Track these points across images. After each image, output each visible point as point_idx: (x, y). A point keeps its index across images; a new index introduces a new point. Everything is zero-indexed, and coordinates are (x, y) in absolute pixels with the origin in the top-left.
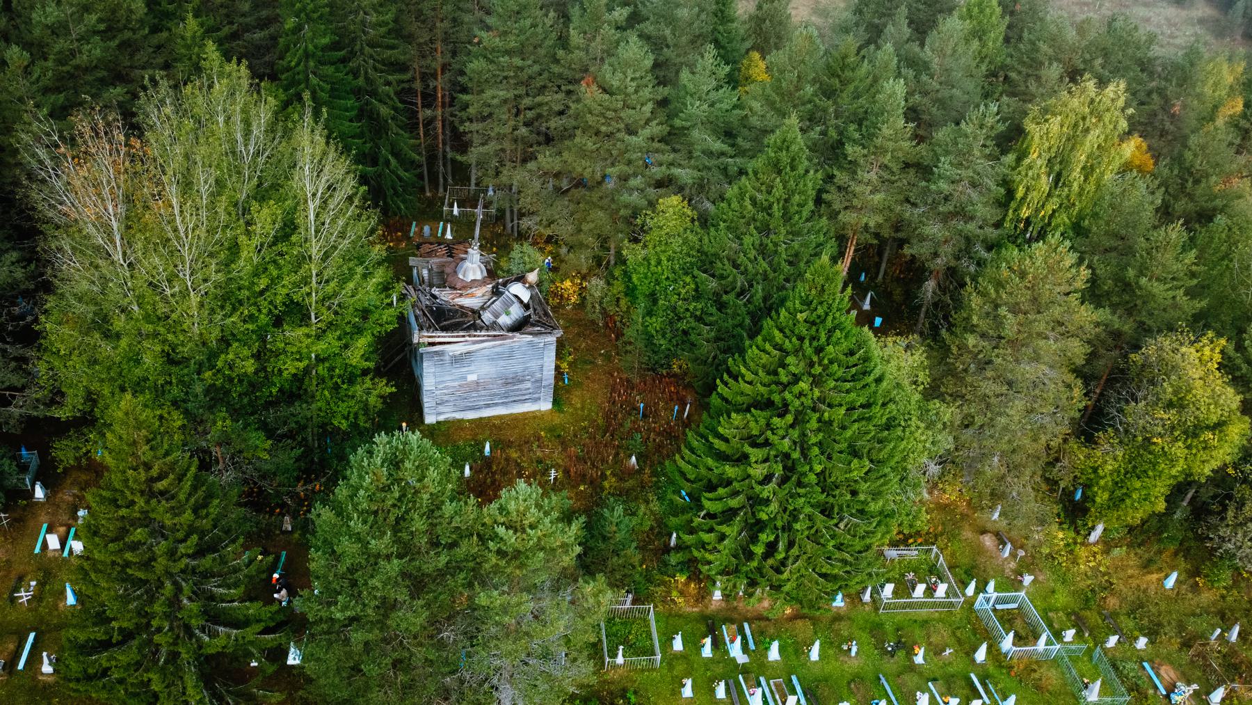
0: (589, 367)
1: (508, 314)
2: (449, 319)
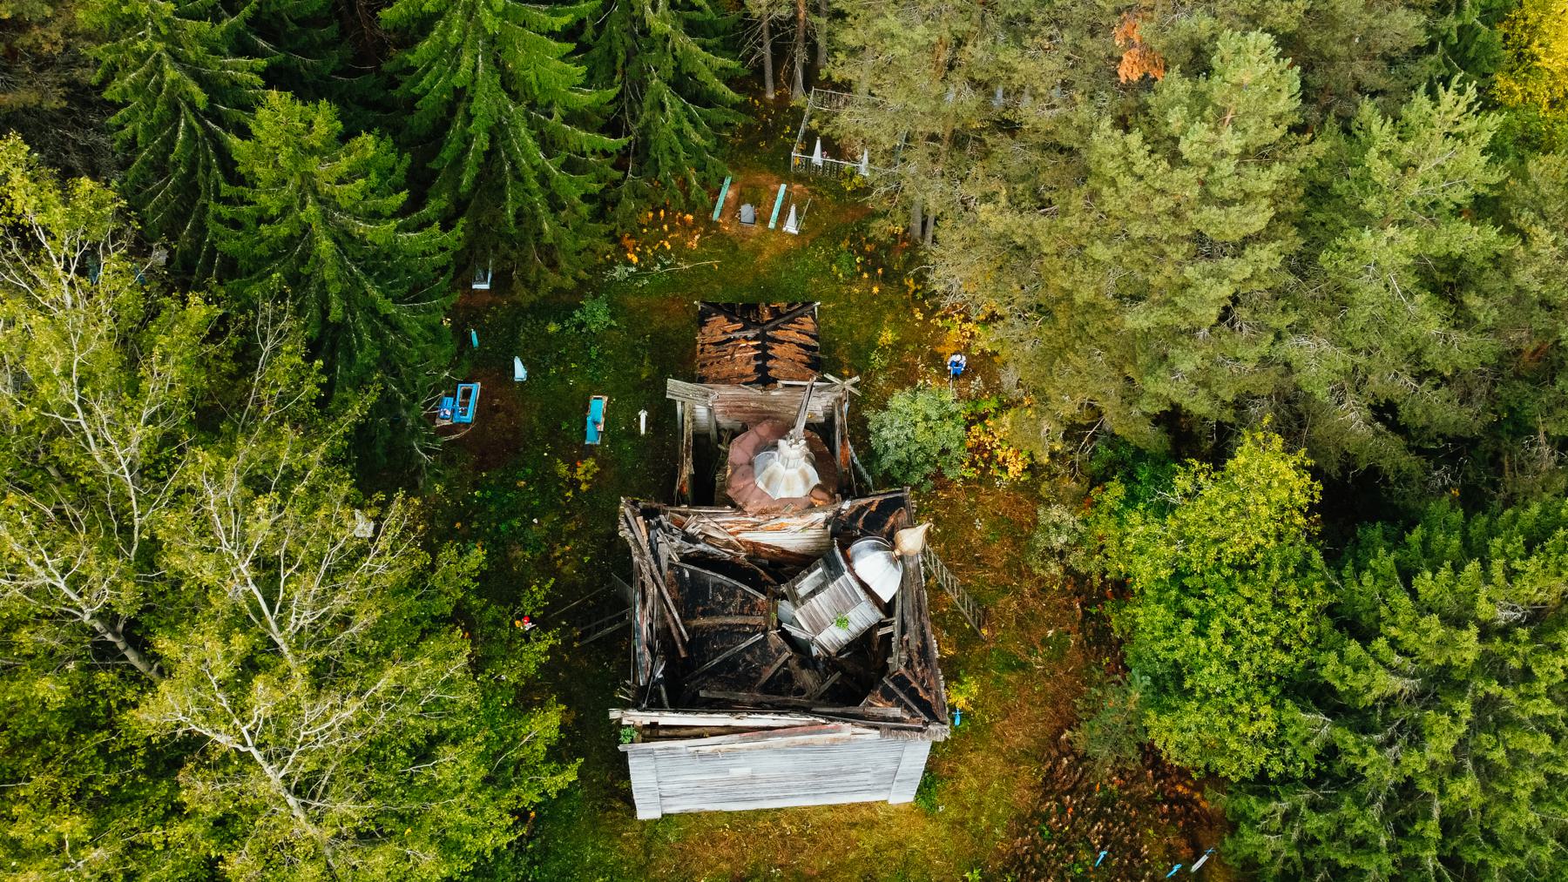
0: (1013, 678)
1: (842, 622)
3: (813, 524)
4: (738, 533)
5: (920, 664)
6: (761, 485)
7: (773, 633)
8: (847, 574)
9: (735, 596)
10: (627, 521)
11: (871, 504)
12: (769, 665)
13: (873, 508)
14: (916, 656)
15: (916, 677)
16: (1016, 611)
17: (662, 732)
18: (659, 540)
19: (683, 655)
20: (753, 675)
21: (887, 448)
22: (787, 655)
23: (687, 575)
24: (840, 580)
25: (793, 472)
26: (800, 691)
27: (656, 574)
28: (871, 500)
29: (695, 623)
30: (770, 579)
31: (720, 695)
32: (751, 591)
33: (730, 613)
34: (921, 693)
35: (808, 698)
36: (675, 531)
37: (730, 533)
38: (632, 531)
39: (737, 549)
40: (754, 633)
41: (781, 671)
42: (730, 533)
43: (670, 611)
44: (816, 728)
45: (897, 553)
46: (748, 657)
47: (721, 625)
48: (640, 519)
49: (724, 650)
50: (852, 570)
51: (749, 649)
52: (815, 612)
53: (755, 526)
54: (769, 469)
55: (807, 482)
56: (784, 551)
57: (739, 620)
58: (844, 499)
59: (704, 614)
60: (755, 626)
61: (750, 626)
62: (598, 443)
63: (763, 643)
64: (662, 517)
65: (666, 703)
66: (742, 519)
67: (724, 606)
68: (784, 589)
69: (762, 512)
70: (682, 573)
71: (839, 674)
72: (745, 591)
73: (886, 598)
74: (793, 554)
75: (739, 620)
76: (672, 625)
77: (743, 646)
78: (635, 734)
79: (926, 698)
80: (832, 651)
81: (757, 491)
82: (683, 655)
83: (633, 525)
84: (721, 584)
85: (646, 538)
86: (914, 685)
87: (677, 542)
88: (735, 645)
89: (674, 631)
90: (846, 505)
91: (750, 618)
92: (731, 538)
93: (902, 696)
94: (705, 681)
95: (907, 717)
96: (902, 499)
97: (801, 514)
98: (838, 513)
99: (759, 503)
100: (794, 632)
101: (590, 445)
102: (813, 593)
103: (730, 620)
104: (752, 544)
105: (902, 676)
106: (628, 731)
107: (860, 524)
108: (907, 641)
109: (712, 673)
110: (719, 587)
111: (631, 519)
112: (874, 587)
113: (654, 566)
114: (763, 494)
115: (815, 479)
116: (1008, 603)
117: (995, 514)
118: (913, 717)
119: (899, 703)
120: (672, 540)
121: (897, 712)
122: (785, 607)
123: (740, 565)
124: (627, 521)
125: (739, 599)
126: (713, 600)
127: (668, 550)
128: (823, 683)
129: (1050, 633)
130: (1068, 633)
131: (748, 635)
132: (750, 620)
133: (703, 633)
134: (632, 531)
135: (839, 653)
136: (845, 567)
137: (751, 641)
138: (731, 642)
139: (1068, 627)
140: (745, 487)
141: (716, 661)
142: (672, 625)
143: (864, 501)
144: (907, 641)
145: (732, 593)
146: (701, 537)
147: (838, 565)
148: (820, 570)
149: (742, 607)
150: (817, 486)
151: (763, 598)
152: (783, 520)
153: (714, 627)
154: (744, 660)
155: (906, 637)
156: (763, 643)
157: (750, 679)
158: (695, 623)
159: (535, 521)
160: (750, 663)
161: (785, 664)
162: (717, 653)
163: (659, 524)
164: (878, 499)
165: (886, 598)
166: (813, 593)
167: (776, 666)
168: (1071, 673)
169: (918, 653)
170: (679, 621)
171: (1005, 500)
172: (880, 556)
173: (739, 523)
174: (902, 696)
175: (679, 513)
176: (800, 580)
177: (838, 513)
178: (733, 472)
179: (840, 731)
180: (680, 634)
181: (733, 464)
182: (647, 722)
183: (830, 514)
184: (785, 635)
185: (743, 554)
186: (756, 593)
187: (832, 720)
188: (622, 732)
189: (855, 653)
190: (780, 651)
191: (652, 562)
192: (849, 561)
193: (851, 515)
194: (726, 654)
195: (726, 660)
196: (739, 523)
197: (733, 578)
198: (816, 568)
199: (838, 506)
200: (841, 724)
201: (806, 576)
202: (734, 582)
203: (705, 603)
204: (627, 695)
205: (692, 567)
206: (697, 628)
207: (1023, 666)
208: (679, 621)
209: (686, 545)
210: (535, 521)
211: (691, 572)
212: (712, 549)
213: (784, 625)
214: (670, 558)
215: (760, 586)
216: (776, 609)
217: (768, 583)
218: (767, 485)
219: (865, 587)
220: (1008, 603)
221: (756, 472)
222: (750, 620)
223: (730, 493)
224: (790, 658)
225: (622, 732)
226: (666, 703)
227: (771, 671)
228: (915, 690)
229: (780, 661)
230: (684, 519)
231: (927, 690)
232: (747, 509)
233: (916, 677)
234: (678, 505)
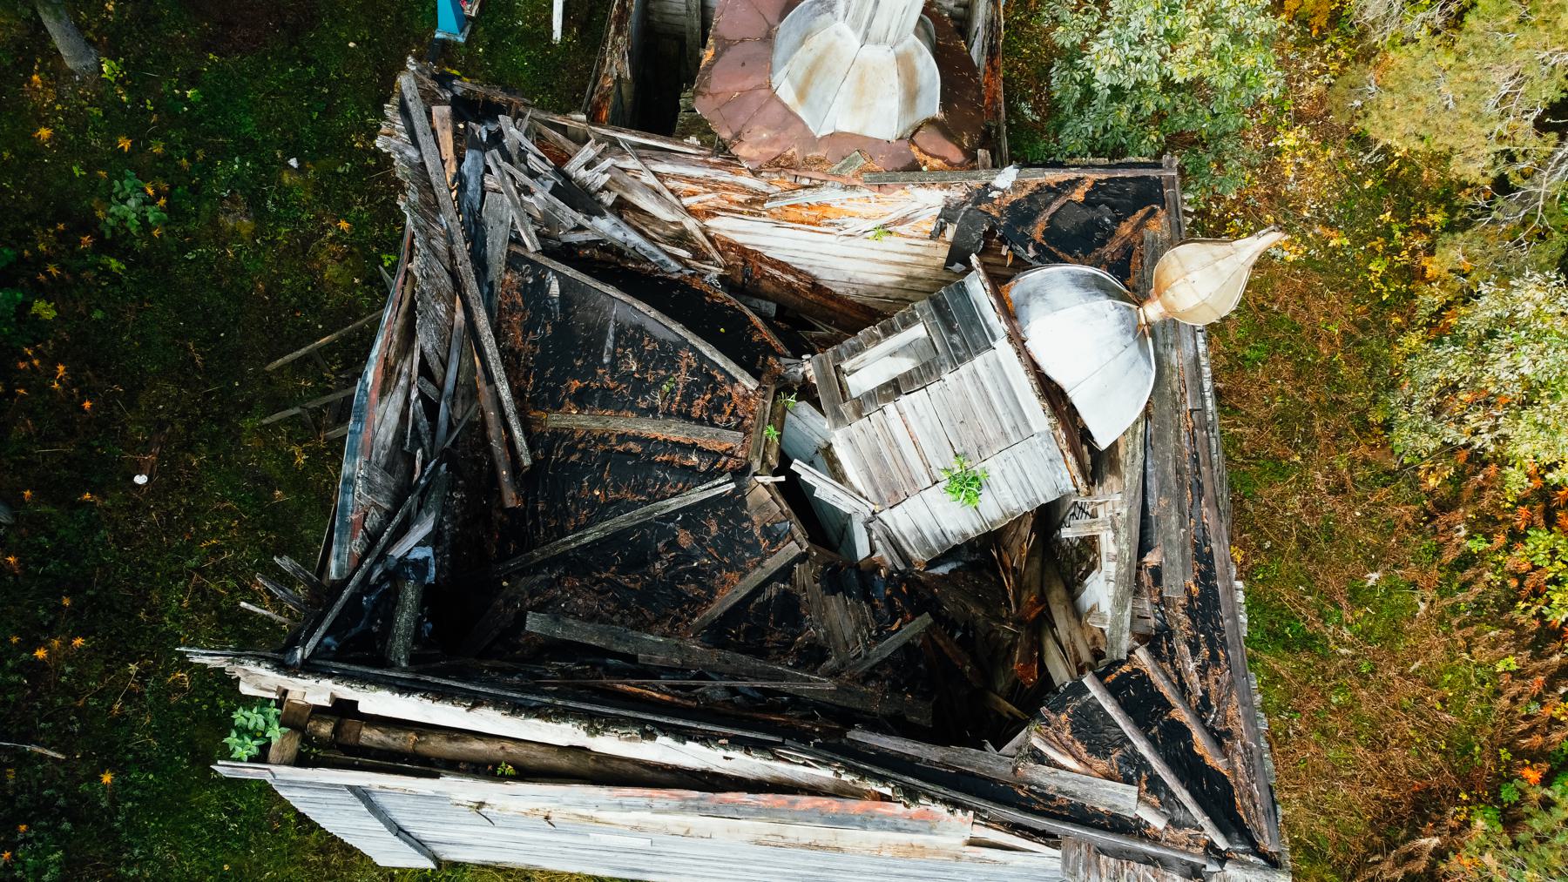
1: (968, 483)
2: (607, 400)
3: (904, 220)
4: (710, 214)
5: (1195, 650)
6: (786, 92)
7: (762, 486)
8: (1003, 349)
9: (673, 366)
10: (404, 111)
11: (1073, 184)
12: (738, 567)
13: (1078, 195)
14: (1182, 623)
15: (1182, 689)
16: (1297, 518)
17: (371, 736)
18: (490, 182)
19: (511, 499)
20: (692, 589)
21: (1089, 94)
22: (792, 549)
23: (555, 289)
24: (978, 361)
25: (881, 57)
26: (814, 656)
27: (466, 268)
28: (1071, 175)
29: (555, 420)
30: (776, 343)
31: (591, 636)
32: (718, 358)
33: (653, 410)
34: (1201, 743)
35: (833, 674)
36: (534, 162)
37: (689, 211)
38: (415, 143)
39: (700, 255)
40: (711, 475)
41: (772, 591)
42: (689, 211)
43: (490, 379)
44: (854, 806)
45: (1153, 311)
46: (685, 539)
47: (623, 438)
48: (441, 112)
49: (621, 506)
50: (1018, 340)
51: (693, 516)
52: (893, 443)
53: (755, 203)
54: (817, 43)
55: (911, 96)
56: (816, 286)
57: (675, 431)
58: (998, 164)
59: (582, 399)
60: (716, 455)
61: (701, 452)
62: (461, 39)
63: (733, 506)
64: (504, 121)
65: (400, 646)
66: (725, 176)
67: (640, 387)
68: (808, 368)
69: (779, 164)
70: (541, 285)
71: (926, 619)
72: (701, 357)
73: (1103, 443)
74: (839, 299)
75: (675, 431)
76: (492, 414)
77: (674, 503)
78: (276, 733)
79: (1217, 762)
80: (918, 556)
81: (775, 109)
82: (511, 499)
83: (420, 123)
84: (639, 328)
85: (451, 169)
86: (1182, 714)
87: (541, 198)
88: (652, 499)
89: (494, 431)
90: (1007, 178)
91: (708, 431)
92: (690, 224)
93: (1143, 748)
94: (557, 582)
95: (1157, 822)
96: (1158, 182)
97: (880, 182)
98: (982, 195)
99: (772, 141)
100: (825, 489)
101: (444, 42)
102: (894, 388)
103: (648, 428)
104: (743, 251)
105: (1142, 679)
106: (254, 719)
107: (1038, 231)
108: (1157, 573)
109: (581, 563)
110: (632, 336)
111: (416, 108)
112: (1078, 398)
113: (462, 249)
114: (789, 116)
115: (931, 105)
116: (1283, 497)
117: (1262, 308)
118: (1173, 823)
119: (1132, 770)
120: (526, 190)
121: (1124, 799)
122: (808, 422)
123: (701, 293)
124: (404, 111)
125: (683, 377)
126: (614, 366)
127: (511, 214)
128: (879, 638)
129: (1373, 578)
130: (1414, 585)
131: (694, 476)
132: (706, 437)
133: (571, 450)
134: (415, 143)
135: (934, 562)
136: (999, 326)
137: (697, 495)
138: (640, 488)
139: (1412, 573)
140: (745, 93)
141: (592, 534)
142: (492, 414)
143: (1052, 177)
144: (1157, 573)
145: (667, 356)
146: (608, 199)
147: (972, 318)
148: (918, 331)
149: (688, 398)
150: (932, 122)
151: (748, 383)
152: (831, 195)
153: (603, 439)
154: (673, 545)
155: (1152, 559)
156: (733, 506)
157: (680, 599)
158: (555, 420)
159: (293, 162)
160: (688, 556)
161: (785, 572)
162: (601, 511)
163: (496, 138)
164: (1093, 176)
165: (1103, 443)
166: (894, 388)
167: (757, 576)
168: (1415, 675)
169: (1189, 611)
170: (510, 408)
171: (1284, 281)
172: (1107, 311)
173: (715, 186)
174: (1143, 748)
175: (563, 130)
176: (857, 350)
177: (982, 195)
178: (717, 56)
179: (930, 831)
180: (510, 443)
181: (719, 39)
182: (324, 701)
183: (958, 194)
184: (795, 493)
185: (715, 271)
186: (732, 368)
187: (912, 795)
188: (239, 717)
189: (971, 567)
190: (775, 537)
191: (459, 236)
192: (1010, 314)
193: (1014, 205)
194: (622, 521)
195: (619, 537)
196: (715, 186)
197: (675, 317)
198: (906, 324)
199: (983, 176)
200: (940, 810)
201: (877, 340)
202: (677, 328)
203: (589, 372)
204: (277, 604)
205: (570, 272)
206: (557, 435)
207: (1308, 642)
208: (510, 408)
209: (569, 215)
210: (293, 162)
211: (565, 282)
212: (634, 238)
213: (797, 466)
214: (517, 241)
215: (750, 357)
216: (778, 418)
217: (769, 350)
218: (802, 94)
219: (1053, 394)
220: (1283, 497)
221: (778, 58)
222: (706, 437)
223: (702, 107)
224: (801, 558)
225: (239, 717)
226: (400, 646)
227: (744, 587)
228: (1181, 731)
229: (773, 564)
230: (570, 146)
231: (1220, 738)
232: (742, 151)
233: (1182, 689)
234: (563, 112)
